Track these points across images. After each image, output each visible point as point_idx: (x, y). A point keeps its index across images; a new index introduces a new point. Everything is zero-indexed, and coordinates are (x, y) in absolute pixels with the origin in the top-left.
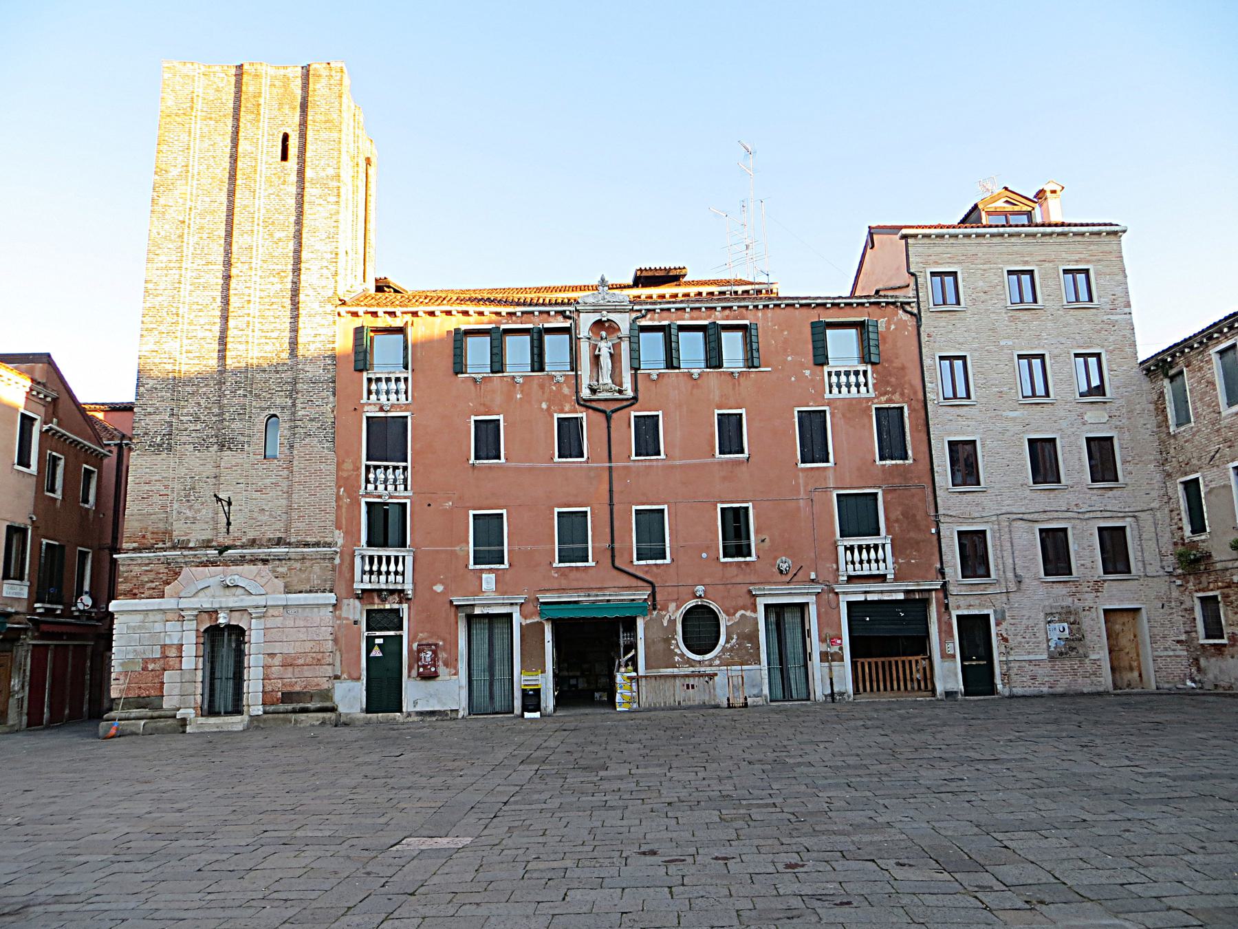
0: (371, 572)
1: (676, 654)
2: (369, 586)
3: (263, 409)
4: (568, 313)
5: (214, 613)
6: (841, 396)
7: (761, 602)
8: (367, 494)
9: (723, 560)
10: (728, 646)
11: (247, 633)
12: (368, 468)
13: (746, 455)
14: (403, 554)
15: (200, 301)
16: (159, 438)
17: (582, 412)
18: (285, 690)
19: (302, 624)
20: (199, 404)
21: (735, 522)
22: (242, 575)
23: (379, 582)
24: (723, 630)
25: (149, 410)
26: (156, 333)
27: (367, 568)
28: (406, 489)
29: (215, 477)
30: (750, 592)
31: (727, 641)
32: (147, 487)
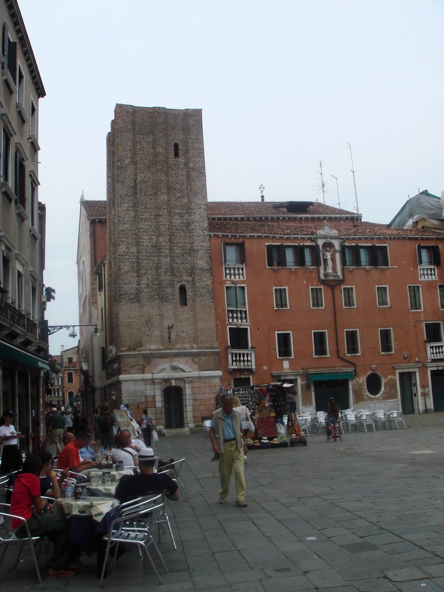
0: (240, 361)
1: (365, 395)
2: (236, 367)
3: (179, 282)
4: (313, 239)
5: (167, 380)
6: (425, 280)
7: (397, 372)
8: (230, 324)
9: (382, 353)
10: (385, 391)
11: (183, 390)
12: (228, 311)
13: (389, 305)
14: (251, 352)
15: (144, 227)
16: (133, 296)
17: (321, 286)
18: (202, 416)
19: (208, 385)
20: (148, 279)
21: (385, 335)
22: (179, 363)
23: (240, 365)
24: (383, 384)
25: (126, 281)
26: (126, 243)
27: (234, 359)
28: (247, 321)
29: (159, 315)
30: (393, 367)
31: (385, 389)
32: (129, 320)
